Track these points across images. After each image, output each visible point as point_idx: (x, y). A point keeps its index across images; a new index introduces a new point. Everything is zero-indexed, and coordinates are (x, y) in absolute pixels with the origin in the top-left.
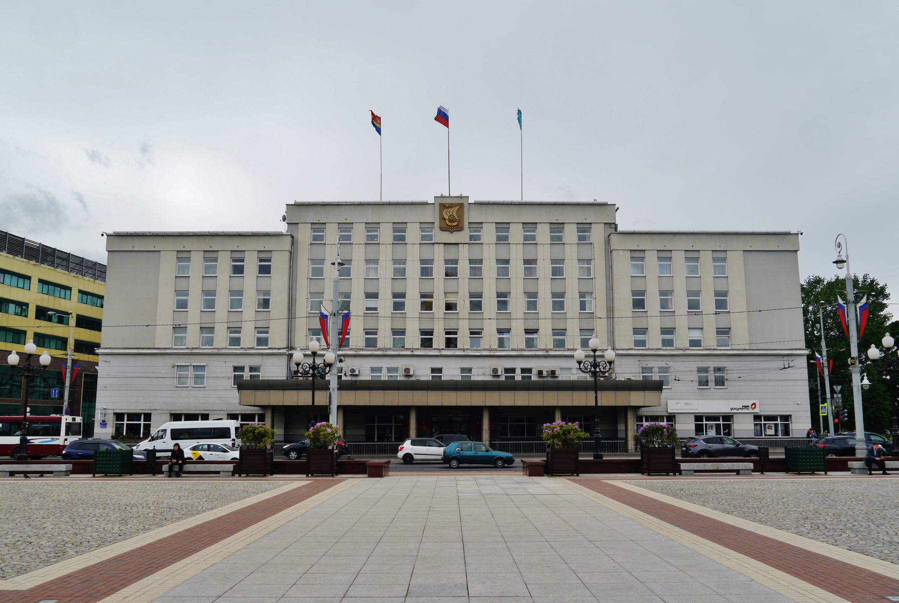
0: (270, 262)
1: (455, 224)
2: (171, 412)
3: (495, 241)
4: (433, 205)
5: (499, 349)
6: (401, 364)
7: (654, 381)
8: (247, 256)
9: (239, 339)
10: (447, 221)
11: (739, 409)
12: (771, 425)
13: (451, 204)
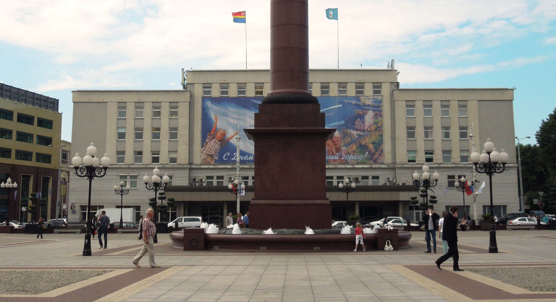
0: (177, 109)
8: (163, 105)
9: (158, 158)
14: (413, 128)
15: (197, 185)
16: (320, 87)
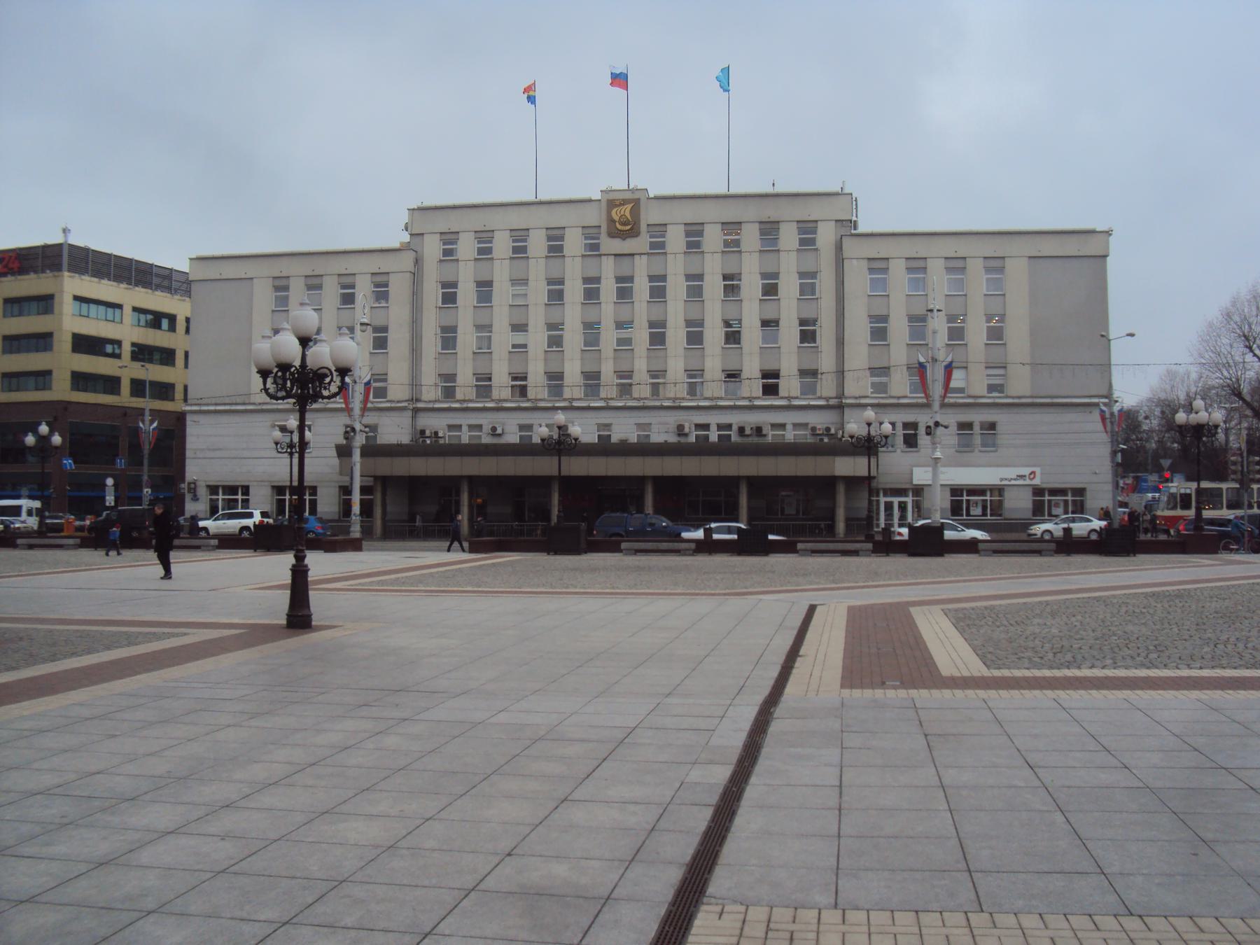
1: (628, 227)
2: (273, 484)
3: (545, 253)
4: (598, 203)
5: (802, 397)
6: (486, 420)
7: (379, 445)
10: (617, 224)
11: (1012, 479)
12: (1059, 502)
13: (623, 200)
14: (884, 319)
15: (428, 442)
16: (683, 234)
